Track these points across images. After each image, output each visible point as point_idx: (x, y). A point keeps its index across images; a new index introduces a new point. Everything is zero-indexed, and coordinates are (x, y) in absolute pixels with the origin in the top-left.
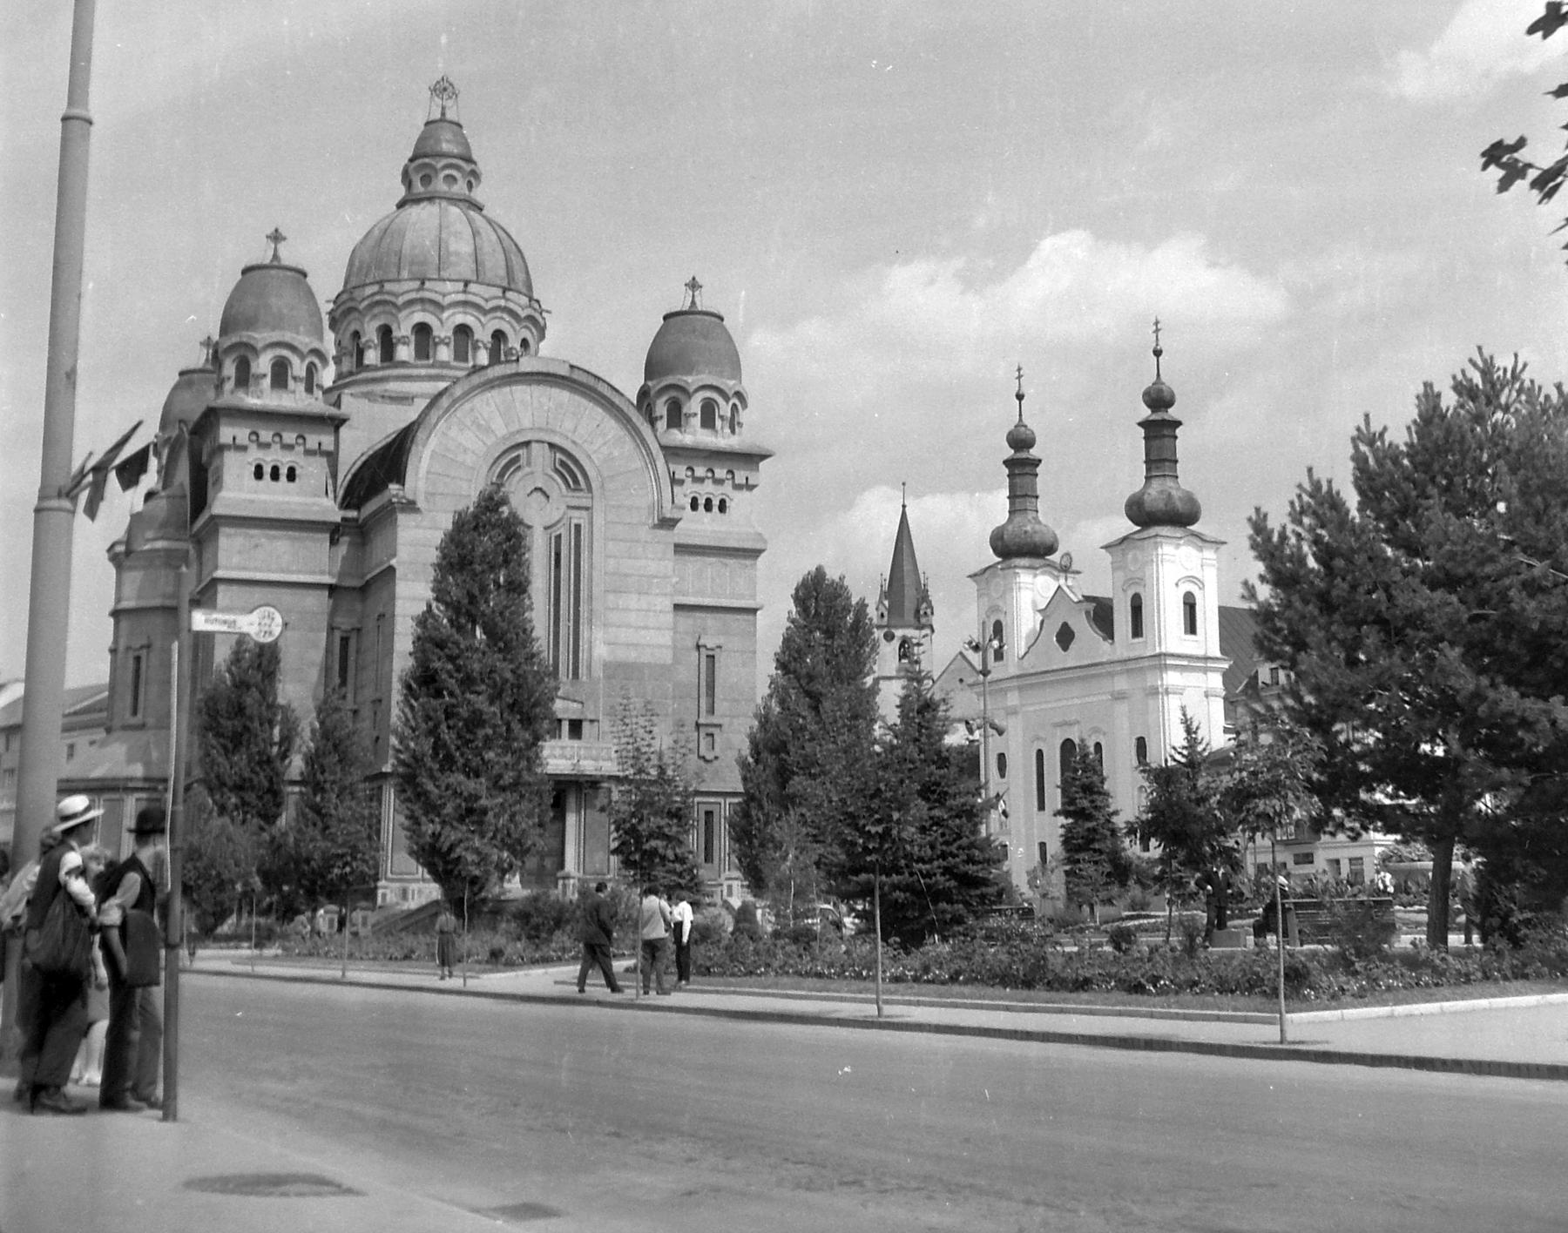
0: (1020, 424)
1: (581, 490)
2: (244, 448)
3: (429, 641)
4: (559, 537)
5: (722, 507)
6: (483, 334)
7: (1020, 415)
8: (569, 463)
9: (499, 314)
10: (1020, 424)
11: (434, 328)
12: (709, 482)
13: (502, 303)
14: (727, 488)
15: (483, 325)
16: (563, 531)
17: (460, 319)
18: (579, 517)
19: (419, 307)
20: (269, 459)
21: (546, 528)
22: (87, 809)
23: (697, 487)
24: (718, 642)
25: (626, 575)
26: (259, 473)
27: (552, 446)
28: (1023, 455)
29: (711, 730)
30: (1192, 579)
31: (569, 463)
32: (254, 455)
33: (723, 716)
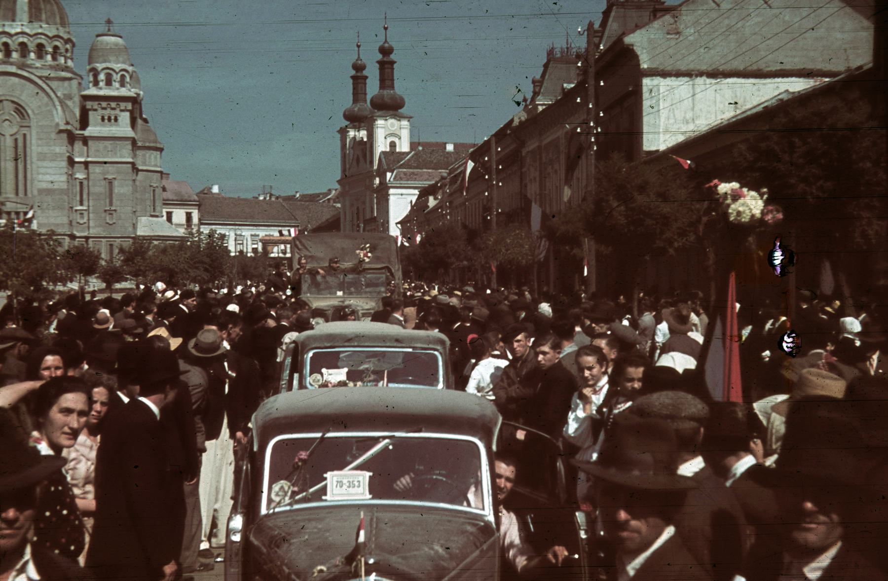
0: (359, 58)
1: (25, 119)
2: (96, 110)
3: (496, 221)
4: (16, 140)
5: (116, 120)
6: (32, 46)
7: (359, 55)
8: (20, 108)
9: (39, 36)
10: (359, 58)
11: (46, 46)
12: (109, 110)
13: (40, 31)
14: (117, 112)
15: (32, 42)
16: (18, 136)
17: (21, 40)
18: (25, 131)
19: (20, 35)
20: (107, 113)
21: (12, 135)
22: (174, 296)
23: (104, 112)
24: (114, 177)
25: (46, 153)
26: (103, 119)
27: (13, 102)
28: (359, 74)
29: (111, 212)
30: (392, 135)
31: (20, 108)
32: (100, 112)
33: (116, 207)
